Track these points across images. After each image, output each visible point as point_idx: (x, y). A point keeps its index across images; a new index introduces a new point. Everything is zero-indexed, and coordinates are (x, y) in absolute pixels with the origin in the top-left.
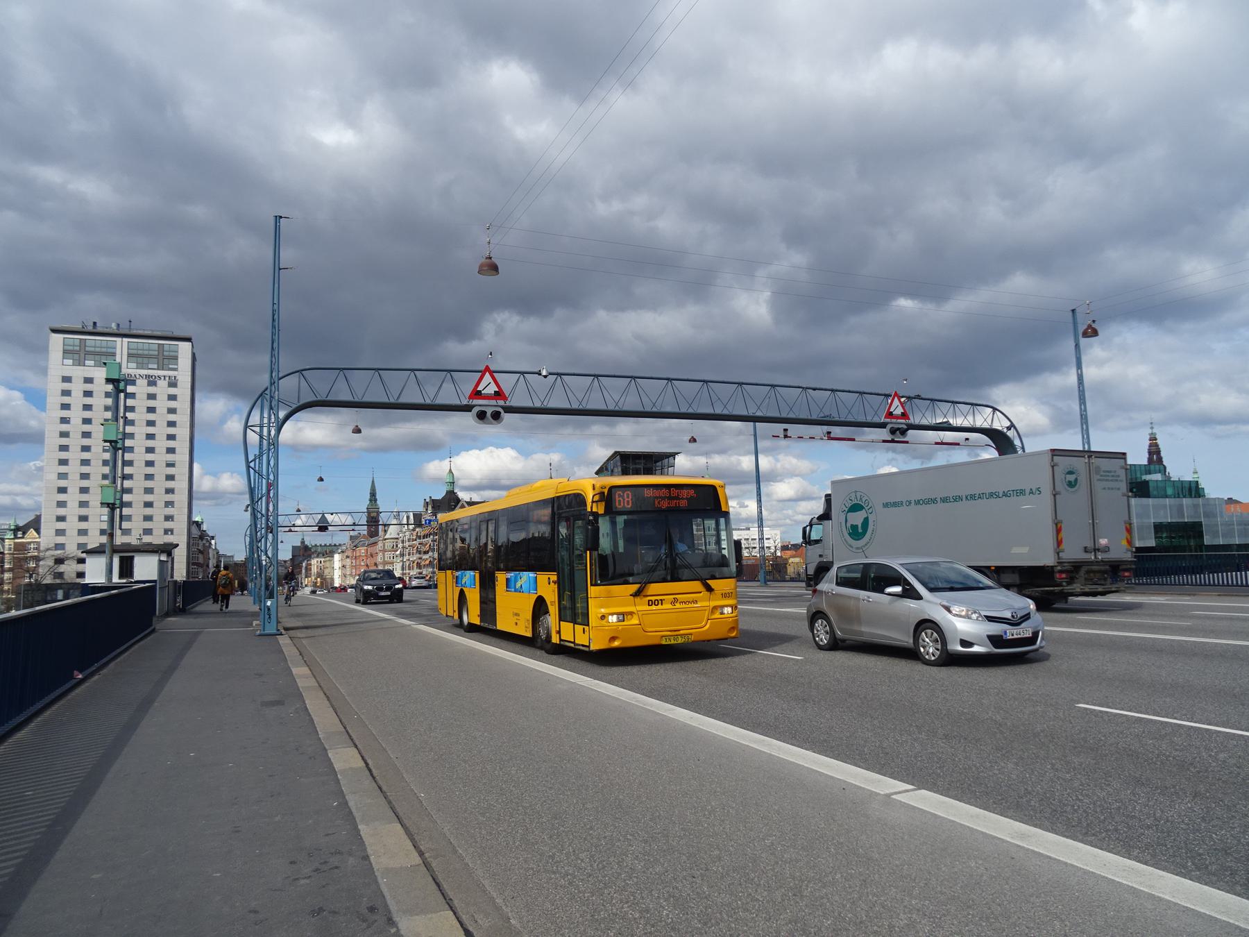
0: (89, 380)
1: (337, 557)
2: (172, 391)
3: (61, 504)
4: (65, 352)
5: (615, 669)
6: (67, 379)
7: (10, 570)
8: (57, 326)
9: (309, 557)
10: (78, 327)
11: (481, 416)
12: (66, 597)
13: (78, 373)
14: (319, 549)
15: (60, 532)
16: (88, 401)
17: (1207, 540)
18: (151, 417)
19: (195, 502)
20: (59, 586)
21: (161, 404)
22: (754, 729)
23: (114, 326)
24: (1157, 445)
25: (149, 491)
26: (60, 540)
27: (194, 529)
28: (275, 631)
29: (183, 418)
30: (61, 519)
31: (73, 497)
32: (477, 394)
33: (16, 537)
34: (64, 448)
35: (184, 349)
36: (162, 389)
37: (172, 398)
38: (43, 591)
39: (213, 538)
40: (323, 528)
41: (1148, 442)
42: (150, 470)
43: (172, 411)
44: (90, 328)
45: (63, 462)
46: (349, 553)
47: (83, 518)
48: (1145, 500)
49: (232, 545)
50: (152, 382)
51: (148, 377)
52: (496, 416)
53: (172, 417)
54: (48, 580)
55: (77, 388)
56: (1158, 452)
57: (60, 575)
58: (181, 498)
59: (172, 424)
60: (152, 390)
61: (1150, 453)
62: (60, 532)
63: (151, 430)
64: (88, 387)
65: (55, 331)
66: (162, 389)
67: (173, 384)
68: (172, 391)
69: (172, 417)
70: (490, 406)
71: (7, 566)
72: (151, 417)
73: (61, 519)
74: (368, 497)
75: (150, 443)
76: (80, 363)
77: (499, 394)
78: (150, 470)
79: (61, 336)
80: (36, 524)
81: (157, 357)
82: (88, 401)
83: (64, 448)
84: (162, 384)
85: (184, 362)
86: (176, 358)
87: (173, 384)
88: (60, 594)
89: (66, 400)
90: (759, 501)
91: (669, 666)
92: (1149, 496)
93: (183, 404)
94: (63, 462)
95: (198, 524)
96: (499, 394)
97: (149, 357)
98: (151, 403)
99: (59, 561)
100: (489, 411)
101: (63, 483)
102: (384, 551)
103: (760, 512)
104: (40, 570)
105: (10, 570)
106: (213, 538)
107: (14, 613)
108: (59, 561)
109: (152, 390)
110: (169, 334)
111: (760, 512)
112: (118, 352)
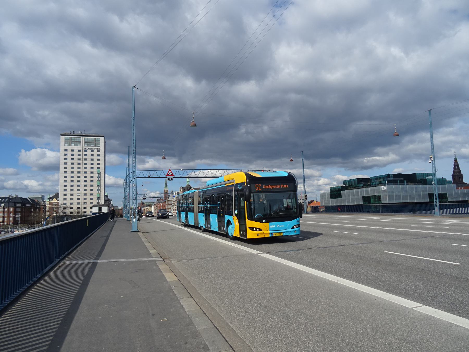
0: (73, 151)
1: (153, 206)
2: (99, 153)
3: (65, 190)
4: (65, 141)
5: (262, 245)
6: (66, 150)
7: (48, 211)
8: (62, 133)
9: (144, 207)
10: (69, 133)
11: (169, 179)
12: (67, 220)
13: (69, 148)
14: (147, 204)
15: (65, 199)
16: (73, 157)
17: (449, 199)
18: (92, 162)
19: (106, 188)
20: (65, 216)
21: (95, 158)
22: (304, 265)
23: (80, 132)
24: (457, 163)
25: (92, 160)
26: (65, 202)
27: (106, 197)
28: (136, 230)
29: (102, 162)
30: (65, 195)
31: (69, 188)
32: (168, 175)
33: (50, 201)
34: (65, 172)
35: (102, 139)
36: (95, 153)
37: (99, 155)
38: (60, 218)
39: (111, 200)
40: (144, 199)
41: (454, 162)
42: (92, 179)
43: (98, 160)
44: (72, 134)
45: (65, 177)
46: (157, 205)
47: (72, 195)
48: (425, 186)
49: (118, 204)
50: (92, 151)
51: (91, 149)
52: (172, 179)
53: (98, 162)
54: (62, 214)
55: (69, 153)
56: (458, 165)
57: (65, 213)
58: (102, 188)
59: (98, 164)
60: (92, 153)
61: (454, 165)
62: (65, 199)
63: (92, 166)
64: (73, 153)
65: (62, 135)
66: (95, 153)
67: (99, 151)
68: (99, 153)
69: (98, 162)
70: (170, 177)
71: (47, 210)
72: (92, 162)
73: (65, 195)
74: (164, 185)
75: (92, 170)
76: (70, 145)
77: (172, 175)
78: (92, 179)
79: (64, 136)
80: (57, 196)
81: (93, 142)
82: (73, 157)
83: (65, 172)
84: (95, 151)
85: (102, 144)
86: (99, 143)
87: (99, 151)
88: (65, 219)
89: (66, 157)
90: (304, 186)
91: (279, 244)
92: (427, 184)
93: (102, 158)
94: (65, 177)
95: (107, 196)
96: (172, 175)
97: (91, 142)
98: (92, 157)
99: (65, 208)
100: (170, 178)
101: (65, 183)
102: (168, 204)
103: (305, 189)
104: (59, 211)
105: (48, 211)
106: (111, 200)
107: (50, 225)
108: (65, 208)
109: (92, 153)
110: (97, 135)
111: (305, 189)
112: (82, 141)
